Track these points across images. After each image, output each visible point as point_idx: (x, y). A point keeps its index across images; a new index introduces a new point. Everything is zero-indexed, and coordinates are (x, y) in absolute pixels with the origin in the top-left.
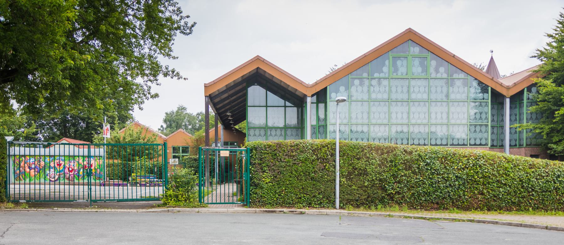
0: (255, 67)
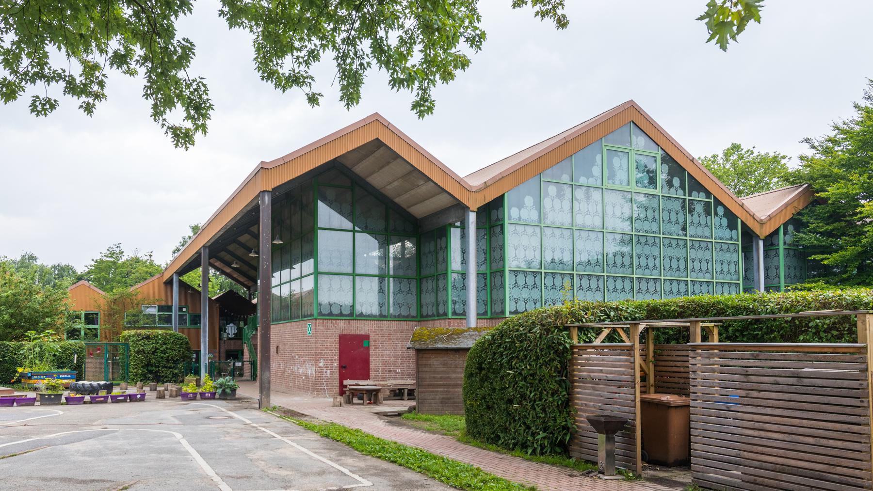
0: (370, 138)
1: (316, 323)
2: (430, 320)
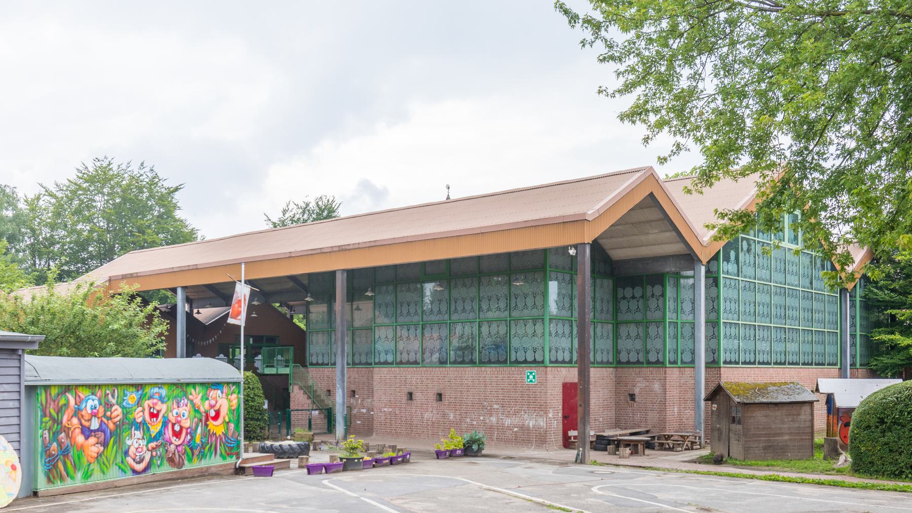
1: (665, 371)
2: (625, 367)
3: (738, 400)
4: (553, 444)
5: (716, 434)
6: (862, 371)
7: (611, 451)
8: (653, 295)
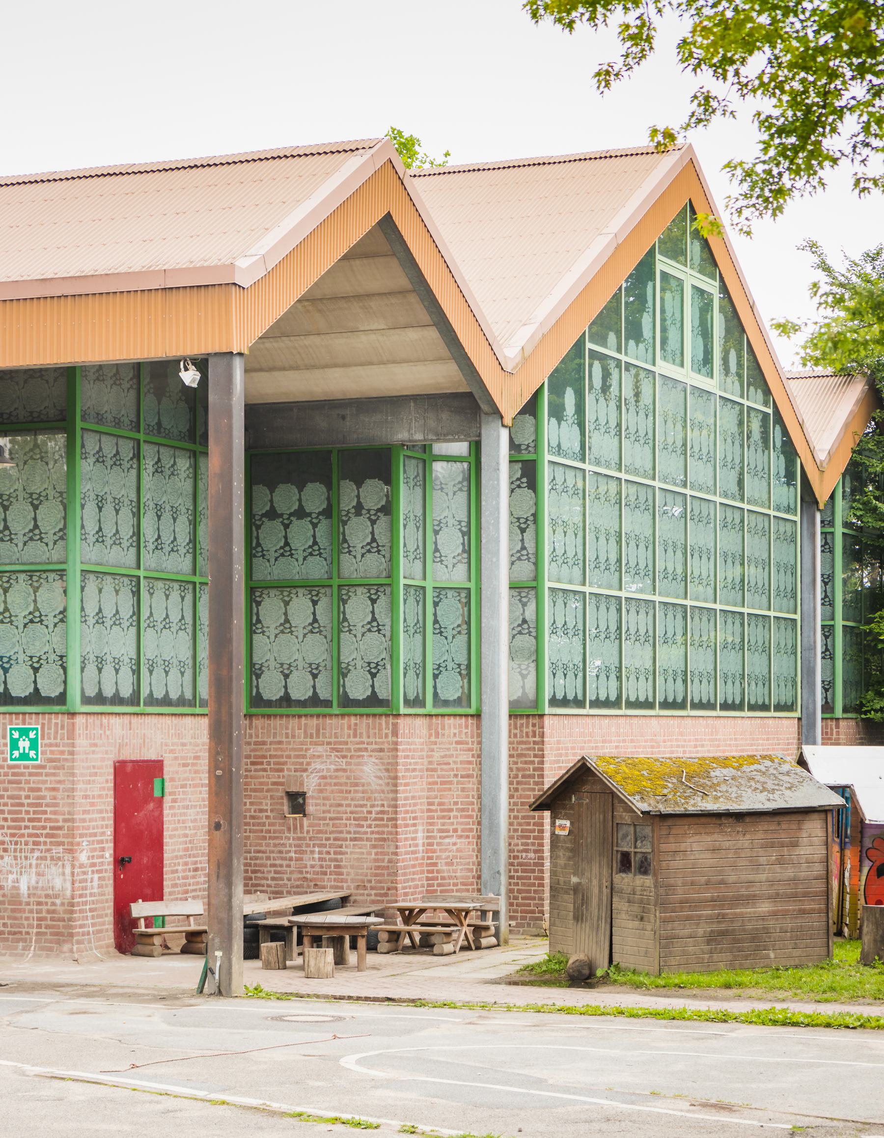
1: (395, 725)
2: (275, 716)
3: (645, 807)
4: (90, 942)
5: (568, 902)
6: (847, 727)
7: (273, 959)
8: (359, 509)
